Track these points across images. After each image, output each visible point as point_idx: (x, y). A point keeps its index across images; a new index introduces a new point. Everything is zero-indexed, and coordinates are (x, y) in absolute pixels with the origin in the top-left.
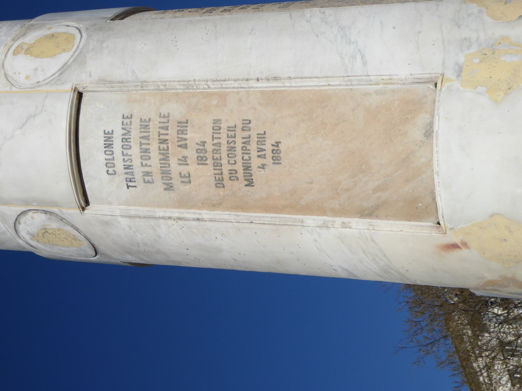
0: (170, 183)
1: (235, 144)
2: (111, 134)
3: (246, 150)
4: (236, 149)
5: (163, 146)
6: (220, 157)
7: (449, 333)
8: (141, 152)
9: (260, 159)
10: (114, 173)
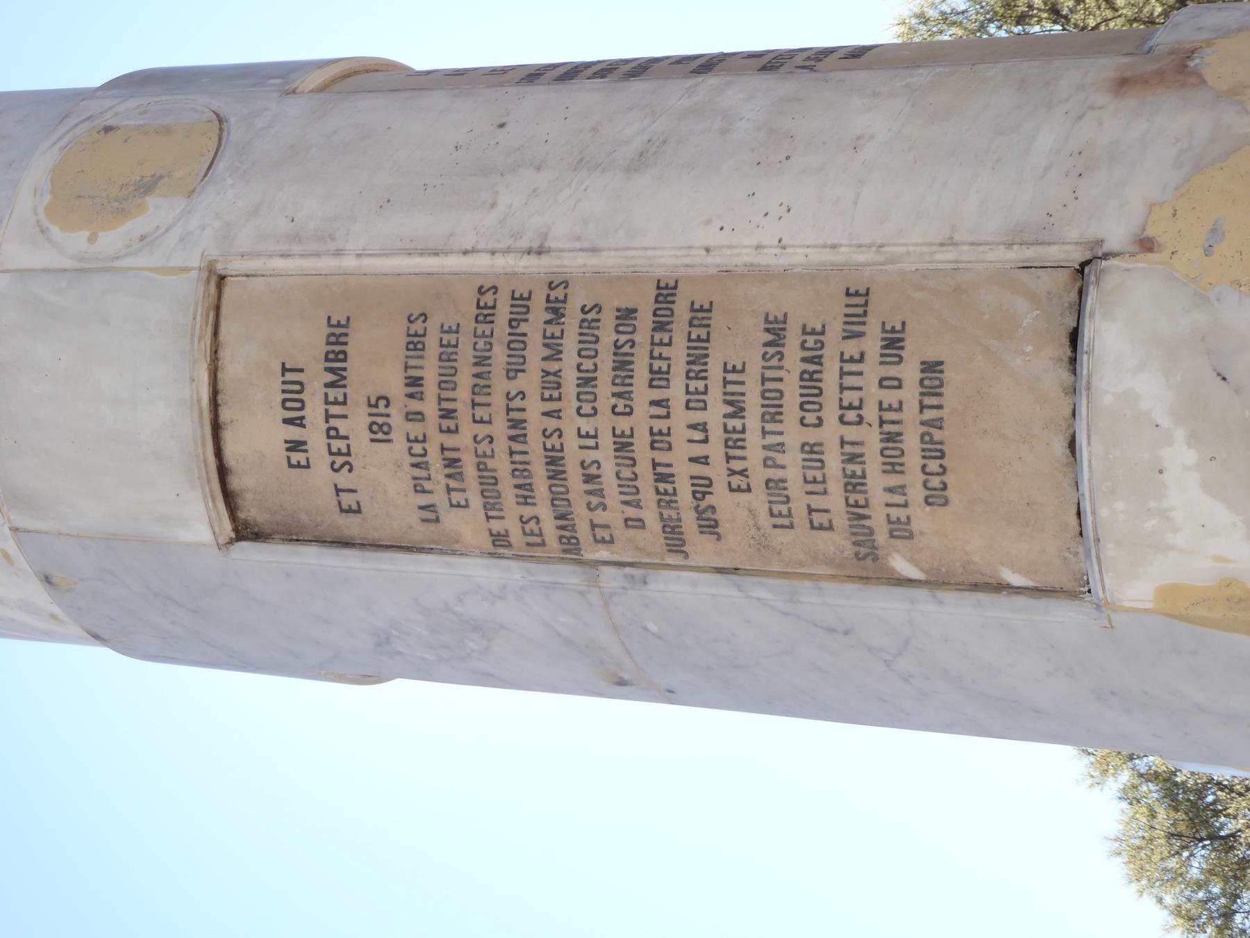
0: (738, 401)
3: (486, 469)
4: (462, 470)
5: (850, 467)
10: (941, 470)
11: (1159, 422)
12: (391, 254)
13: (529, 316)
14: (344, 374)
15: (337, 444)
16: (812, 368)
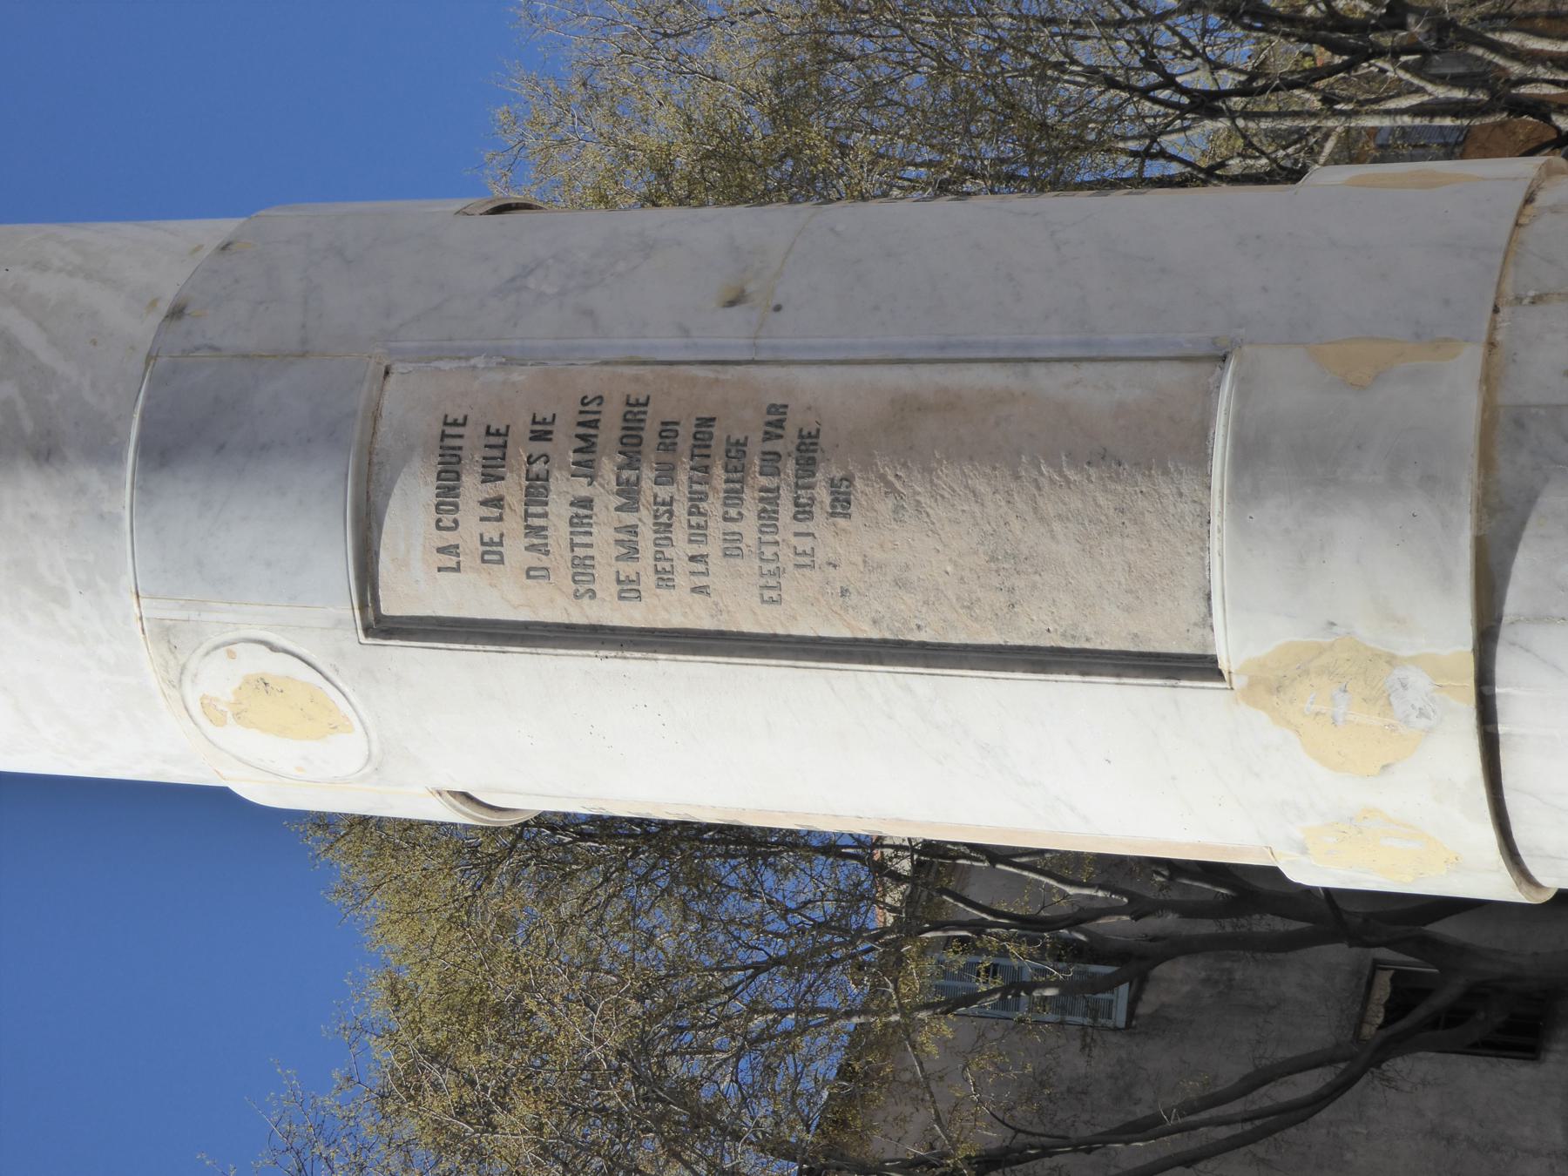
8: (438, 496)
15: (694, 520)
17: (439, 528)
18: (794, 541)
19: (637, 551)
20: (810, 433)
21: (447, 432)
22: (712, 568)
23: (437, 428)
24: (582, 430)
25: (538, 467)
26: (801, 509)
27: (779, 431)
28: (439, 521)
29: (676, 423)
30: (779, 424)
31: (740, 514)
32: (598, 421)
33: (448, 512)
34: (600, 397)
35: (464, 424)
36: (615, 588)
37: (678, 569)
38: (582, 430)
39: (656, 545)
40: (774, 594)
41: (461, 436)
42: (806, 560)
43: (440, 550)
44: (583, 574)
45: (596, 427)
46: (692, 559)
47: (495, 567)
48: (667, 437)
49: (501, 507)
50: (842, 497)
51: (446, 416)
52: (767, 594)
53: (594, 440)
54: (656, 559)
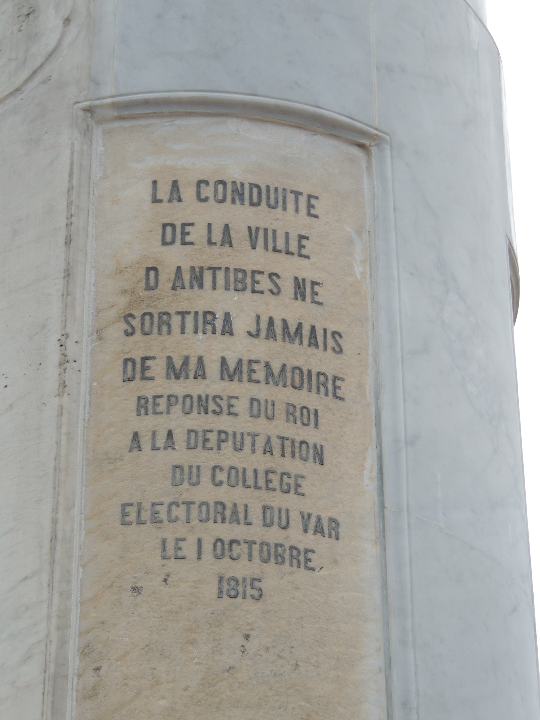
1: (214, 412)
2: (183, 239)
6: (161, 413)
7: (255, 505)
8: (234, 183)
9: (131, 437)
11: (83, 130)
12: (255, 382)
13: (312, 408)
14: (236, 378)
15: (213, 437)
16: (219, 324)
17: (214, 468)
18: (192, 540)
19: (177, 378)
20: (310, 560)
21: (300, 197)
22: (161, 453)
23: (305, 188)
24: (306, 331)
25: (265, 284)
26: (227, 546)
27: (313, 520)
28: (207, 183)
29: (316, 425)
30: (319, 530)
31: (221, 483)
32: (317, 346)
33: (216, 191)
34: (341, 351)
35: (309, 214)
36: (137, 356)
37: (160, 419)
38: (306, 331)
39: (185, 397)
40: (133, 517)
41: (297, 210)
42: (170, 551)
43: (175, 184)
44: (152, 323)
45: (310, 345)
46: (170, 434)
47: (160, 237)
48: (302, 414)
49: (223, 244)
50: (240, 589)
51: (317, 198)
52: (132, 511)
53: (297, 341)
54: (169, 397)
